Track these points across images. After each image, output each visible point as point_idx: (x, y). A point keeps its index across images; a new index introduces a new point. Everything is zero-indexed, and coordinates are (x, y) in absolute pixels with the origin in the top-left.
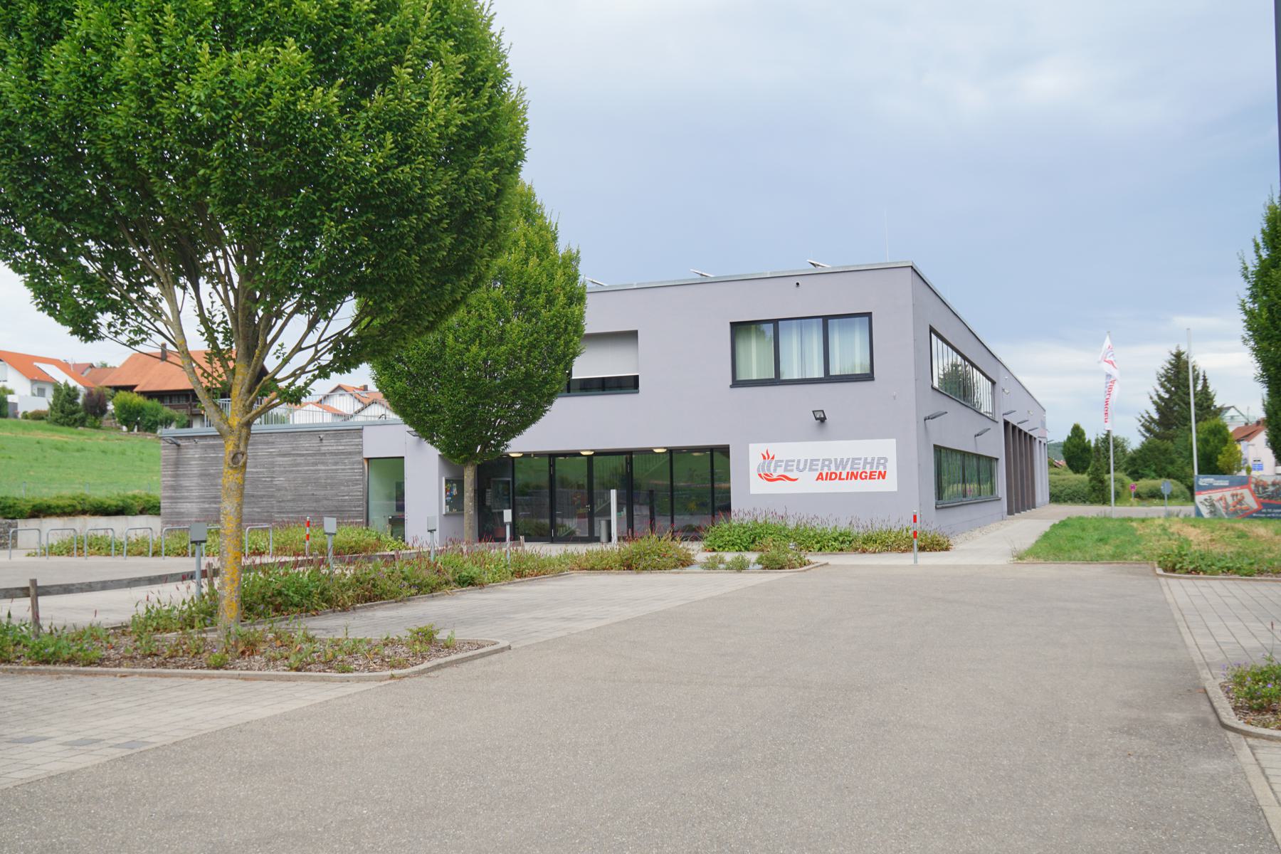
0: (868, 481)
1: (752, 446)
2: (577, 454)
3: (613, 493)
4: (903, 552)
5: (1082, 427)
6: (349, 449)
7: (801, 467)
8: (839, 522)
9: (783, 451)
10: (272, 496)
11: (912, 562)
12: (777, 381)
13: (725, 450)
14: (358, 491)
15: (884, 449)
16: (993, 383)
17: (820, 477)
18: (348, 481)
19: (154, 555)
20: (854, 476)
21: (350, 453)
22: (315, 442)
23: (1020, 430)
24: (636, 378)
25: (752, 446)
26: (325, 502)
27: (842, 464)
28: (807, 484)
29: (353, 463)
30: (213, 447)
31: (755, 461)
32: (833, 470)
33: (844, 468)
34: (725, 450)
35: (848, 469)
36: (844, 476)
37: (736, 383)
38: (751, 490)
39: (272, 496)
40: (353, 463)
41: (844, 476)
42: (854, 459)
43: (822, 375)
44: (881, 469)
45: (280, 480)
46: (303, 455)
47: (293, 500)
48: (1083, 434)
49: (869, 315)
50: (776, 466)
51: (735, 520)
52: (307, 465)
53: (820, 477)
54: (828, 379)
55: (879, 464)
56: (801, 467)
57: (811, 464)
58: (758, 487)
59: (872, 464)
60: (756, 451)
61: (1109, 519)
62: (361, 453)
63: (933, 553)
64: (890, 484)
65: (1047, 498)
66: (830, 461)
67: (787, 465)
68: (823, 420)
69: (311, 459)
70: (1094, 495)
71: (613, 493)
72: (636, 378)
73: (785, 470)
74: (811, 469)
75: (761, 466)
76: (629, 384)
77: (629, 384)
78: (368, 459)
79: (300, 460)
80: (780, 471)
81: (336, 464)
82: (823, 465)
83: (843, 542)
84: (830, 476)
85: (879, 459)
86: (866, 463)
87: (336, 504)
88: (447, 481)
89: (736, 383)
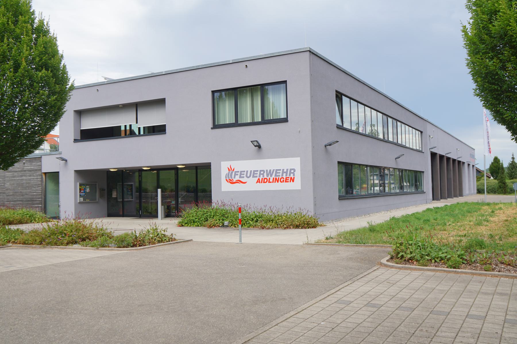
1: (223, 163)
4: (285, 228)
5: (499, 157)
7: (248, 175)
8: (253, 207)
9: (239, 165)
10: (4, 193)
12: (236, 124)
13: (207, 167)
14: (39, 190)
15: (293, 163)
16: (421, 132)
17: (259, 181)
18: (36, 185)
20: (276, 180)
21: (36, 170)
23: (448, 159)
24: (164, 126)
25: (223, 163)
26: (26, 196)
27: (270, 173)
28: (252, 185)
29: (37, 176)
31: (224, 172)
32: (265, 177)
33: (271, 176)
34: (207, 167)
36: (271, 180)
37: (215, 126)
38: (222, 189)
39: (4, 193)
40: (37, 176)
41: (271, 180)
42: (277, 170)
43: (260, 120)
44: (292, 176)
45: (7, 185)
46: (16, 172)
47: (13, 195)
48: (499, 161)
49: (285, 82)
50: (235, 175)
51: (213, 204)
52: (18, 177)
53: (259, 181)
54: (265, 122)
55: (290, 173)
56: (248, 175)
57: (254, 174)
58: (226, 187)
59: (286, 173)
60: (225, 166)
61: (22, 232)
62: (41, 170)
63: (264, 231)
64: (296, 185)
65: (476, 191)
66: (263, 171)
67: (241, 174)
68: (259, 147)
69: (20, 174)
70: (500, 190)
72: (164, 126)
73: (240, 177)
74: (254, 177)
75: (227, 175)
76: (160, 130)
77: (160, 130)
78: (45, 173)
79: (16, 174)
80: (237, 178)
81: (30, 176)
82: (260, 174)
83: (257, 221)
84: (264, 181)
85: (291, 170)
86: (283, 172)
87: (30, 197)
88: (81, 185)
89: (215, 126)
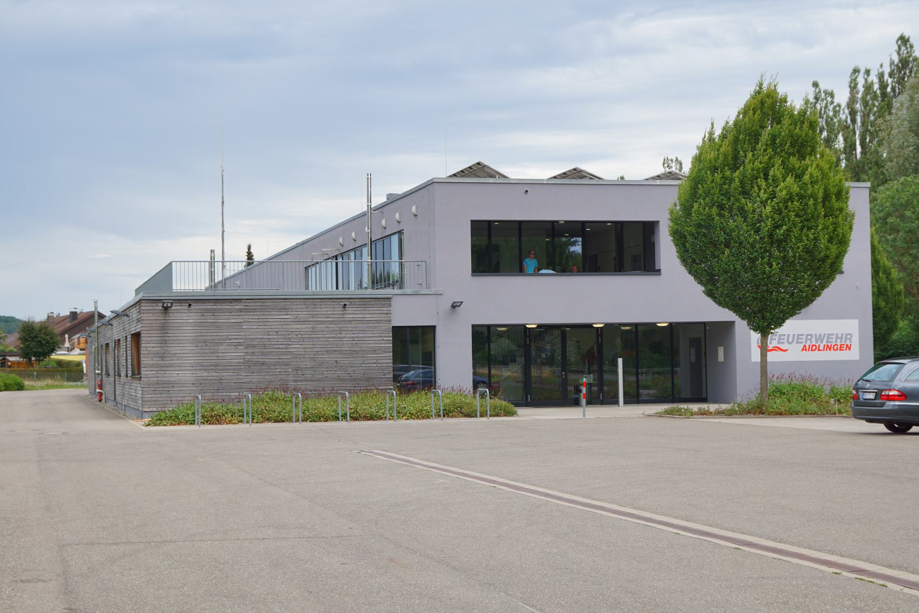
0: (838, 352)
2: (589, 326)
3: (620, 361)
6: (376, 317)
7: (790, 340)
11: (581, 417)
16: (307, 268)
17: (804, 348)
19: (481, 416)
20: (828, 348)
22: (339, 310)
27: (820, 338)
30: (213, 312)
33: (821, 342)
35: (824, 342)
36: (821, 348)
41: (821, 348)
42: (799, 335)
45: (296, 348)
53: (804, 348)
55: (846, 339)
56: (790, 340)
59: (841, 338)
62: (390, 321)
64: (853, 355)
66: (811, 335)
71: (620, 361)
73: (779, 343)
74: (797, 342)
82: (807, 339)
84: (813, 348)
85: (847, 334)
86: (837, 338)
